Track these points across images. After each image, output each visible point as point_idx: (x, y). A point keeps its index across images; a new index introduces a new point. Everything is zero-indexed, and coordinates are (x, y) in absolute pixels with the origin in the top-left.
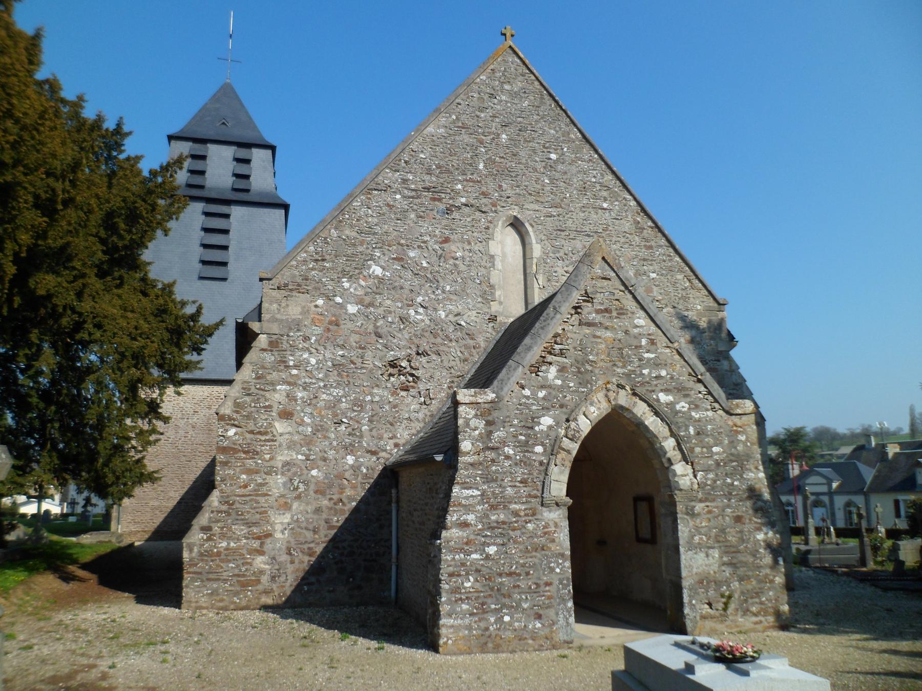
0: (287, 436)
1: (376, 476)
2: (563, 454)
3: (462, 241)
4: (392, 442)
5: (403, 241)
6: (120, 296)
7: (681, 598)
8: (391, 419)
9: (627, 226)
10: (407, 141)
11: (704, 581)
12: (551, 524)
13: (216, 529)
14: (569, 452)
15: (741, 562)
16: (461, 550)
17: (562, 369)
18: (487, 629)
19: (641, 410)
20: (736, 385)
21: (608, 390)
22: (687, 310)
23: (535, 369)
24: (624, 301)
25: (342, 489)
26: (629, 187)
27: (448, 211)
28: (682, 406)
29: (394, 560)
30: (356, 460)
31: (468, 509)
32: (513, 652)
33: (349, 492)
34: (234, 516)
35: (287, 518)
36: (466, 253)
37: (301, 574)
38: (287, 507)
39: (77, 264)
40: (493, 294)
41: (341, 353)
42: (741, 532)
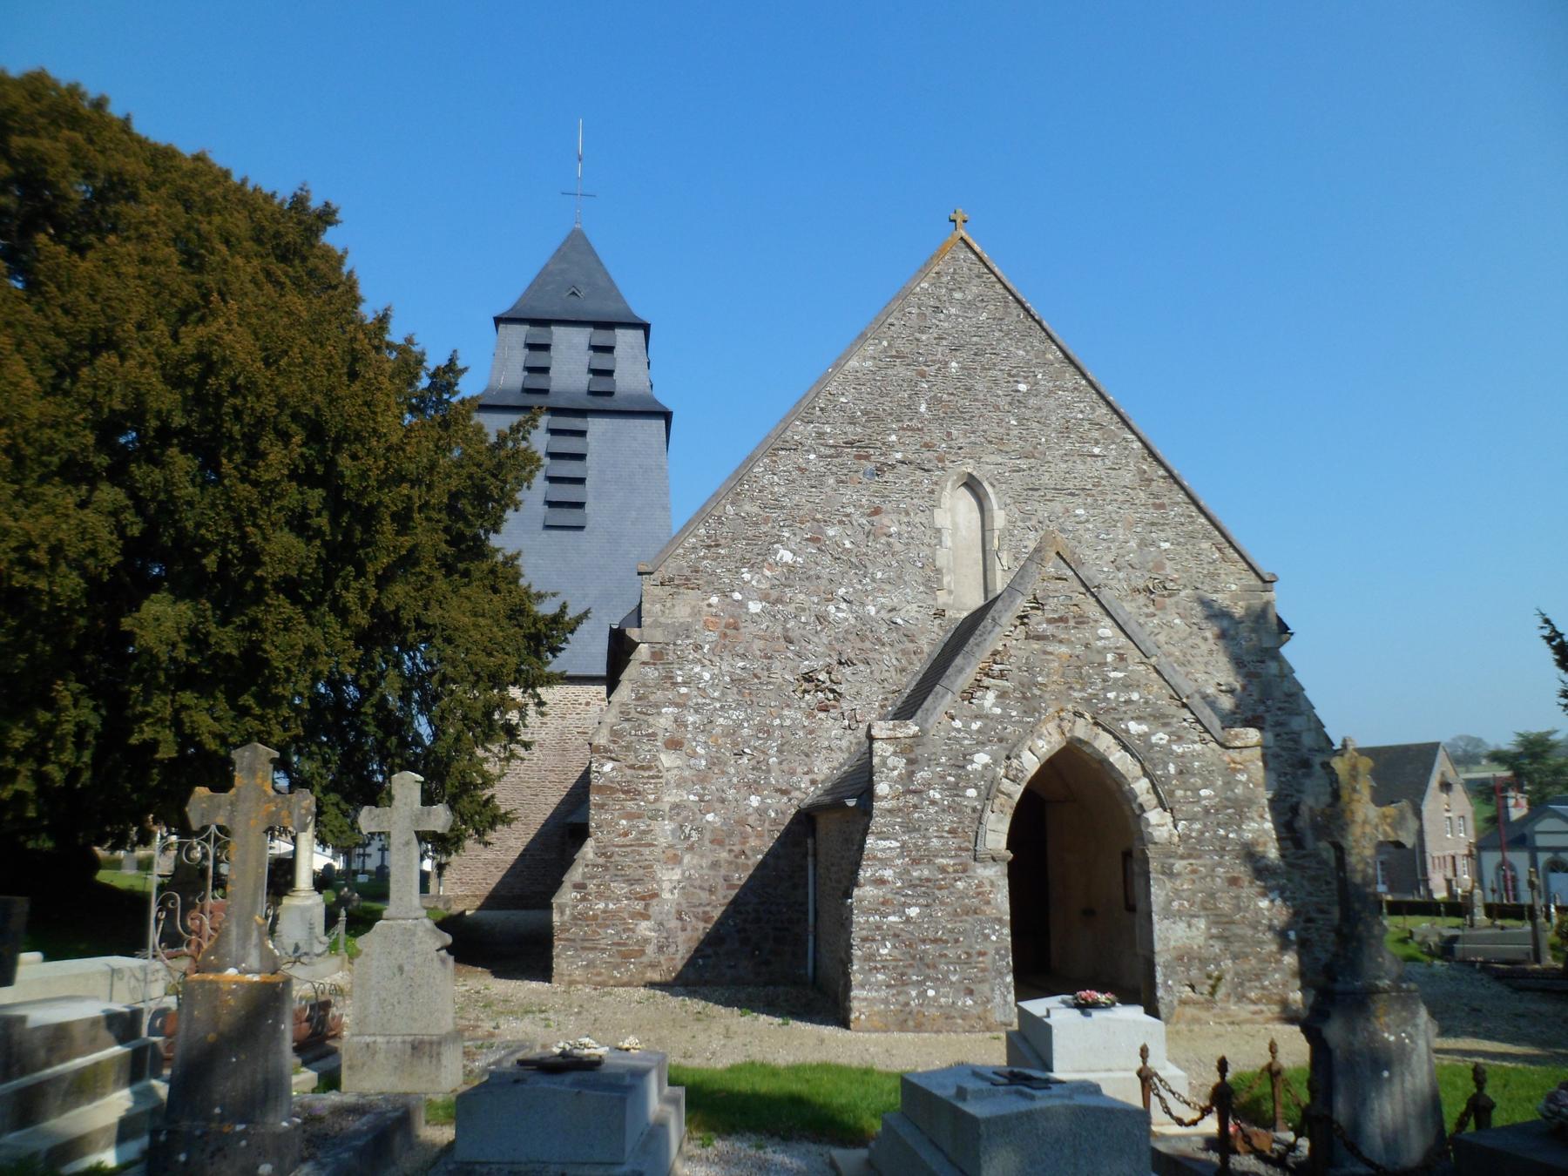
0: (675, 772)
1: (787, 821)
2: (1002, 798)
3: (898, 511)
4: (807, 778)
5: (819, 516)
6: (468, 598)
7: (1154, 977)
8: (805, 749)
9: (1128, 477)
10: (823, 380)
11: (1184, 957)
12: (986, 882)
13: (591, 887)
14: (1009, 796)
15: (1236, 935)
16: (876, 911)
17: (1003, 695)
18: (907, 1004)
19: (1104, 743)
20: (1289, 695)
21: (1062, 719)
22: (1216, 591)
23: (968, 696)
24: (1084, 607)
25: (744, 838)
26: (1132, 423)
27: (879, 471)
28: (1160, 737)
29: (811, 929)
30: (762, 801)
31: (885, 863)
32: (939, 1031)
33: (753, 842)
34: (612, 871)
35: (676, 875)
36: (904, 527)
37: (694, 945)
38: (676, 860)
39: (425, 568)
40: (939, 581)
41: (741, 664)
42: (1237, 897)
